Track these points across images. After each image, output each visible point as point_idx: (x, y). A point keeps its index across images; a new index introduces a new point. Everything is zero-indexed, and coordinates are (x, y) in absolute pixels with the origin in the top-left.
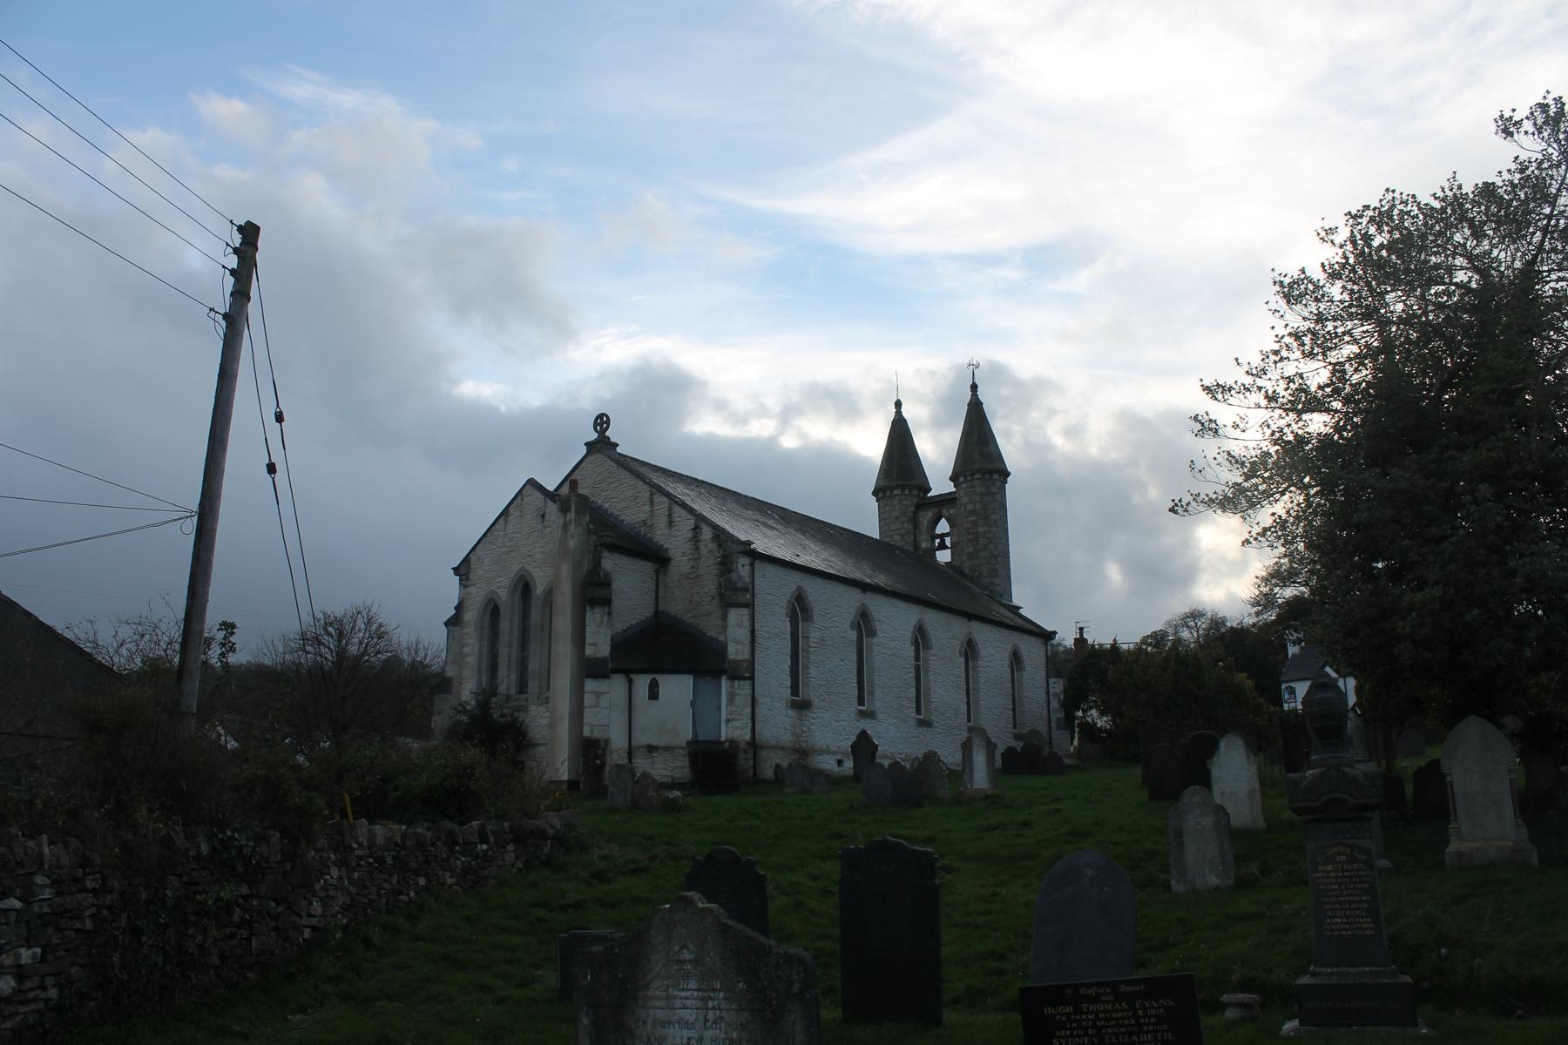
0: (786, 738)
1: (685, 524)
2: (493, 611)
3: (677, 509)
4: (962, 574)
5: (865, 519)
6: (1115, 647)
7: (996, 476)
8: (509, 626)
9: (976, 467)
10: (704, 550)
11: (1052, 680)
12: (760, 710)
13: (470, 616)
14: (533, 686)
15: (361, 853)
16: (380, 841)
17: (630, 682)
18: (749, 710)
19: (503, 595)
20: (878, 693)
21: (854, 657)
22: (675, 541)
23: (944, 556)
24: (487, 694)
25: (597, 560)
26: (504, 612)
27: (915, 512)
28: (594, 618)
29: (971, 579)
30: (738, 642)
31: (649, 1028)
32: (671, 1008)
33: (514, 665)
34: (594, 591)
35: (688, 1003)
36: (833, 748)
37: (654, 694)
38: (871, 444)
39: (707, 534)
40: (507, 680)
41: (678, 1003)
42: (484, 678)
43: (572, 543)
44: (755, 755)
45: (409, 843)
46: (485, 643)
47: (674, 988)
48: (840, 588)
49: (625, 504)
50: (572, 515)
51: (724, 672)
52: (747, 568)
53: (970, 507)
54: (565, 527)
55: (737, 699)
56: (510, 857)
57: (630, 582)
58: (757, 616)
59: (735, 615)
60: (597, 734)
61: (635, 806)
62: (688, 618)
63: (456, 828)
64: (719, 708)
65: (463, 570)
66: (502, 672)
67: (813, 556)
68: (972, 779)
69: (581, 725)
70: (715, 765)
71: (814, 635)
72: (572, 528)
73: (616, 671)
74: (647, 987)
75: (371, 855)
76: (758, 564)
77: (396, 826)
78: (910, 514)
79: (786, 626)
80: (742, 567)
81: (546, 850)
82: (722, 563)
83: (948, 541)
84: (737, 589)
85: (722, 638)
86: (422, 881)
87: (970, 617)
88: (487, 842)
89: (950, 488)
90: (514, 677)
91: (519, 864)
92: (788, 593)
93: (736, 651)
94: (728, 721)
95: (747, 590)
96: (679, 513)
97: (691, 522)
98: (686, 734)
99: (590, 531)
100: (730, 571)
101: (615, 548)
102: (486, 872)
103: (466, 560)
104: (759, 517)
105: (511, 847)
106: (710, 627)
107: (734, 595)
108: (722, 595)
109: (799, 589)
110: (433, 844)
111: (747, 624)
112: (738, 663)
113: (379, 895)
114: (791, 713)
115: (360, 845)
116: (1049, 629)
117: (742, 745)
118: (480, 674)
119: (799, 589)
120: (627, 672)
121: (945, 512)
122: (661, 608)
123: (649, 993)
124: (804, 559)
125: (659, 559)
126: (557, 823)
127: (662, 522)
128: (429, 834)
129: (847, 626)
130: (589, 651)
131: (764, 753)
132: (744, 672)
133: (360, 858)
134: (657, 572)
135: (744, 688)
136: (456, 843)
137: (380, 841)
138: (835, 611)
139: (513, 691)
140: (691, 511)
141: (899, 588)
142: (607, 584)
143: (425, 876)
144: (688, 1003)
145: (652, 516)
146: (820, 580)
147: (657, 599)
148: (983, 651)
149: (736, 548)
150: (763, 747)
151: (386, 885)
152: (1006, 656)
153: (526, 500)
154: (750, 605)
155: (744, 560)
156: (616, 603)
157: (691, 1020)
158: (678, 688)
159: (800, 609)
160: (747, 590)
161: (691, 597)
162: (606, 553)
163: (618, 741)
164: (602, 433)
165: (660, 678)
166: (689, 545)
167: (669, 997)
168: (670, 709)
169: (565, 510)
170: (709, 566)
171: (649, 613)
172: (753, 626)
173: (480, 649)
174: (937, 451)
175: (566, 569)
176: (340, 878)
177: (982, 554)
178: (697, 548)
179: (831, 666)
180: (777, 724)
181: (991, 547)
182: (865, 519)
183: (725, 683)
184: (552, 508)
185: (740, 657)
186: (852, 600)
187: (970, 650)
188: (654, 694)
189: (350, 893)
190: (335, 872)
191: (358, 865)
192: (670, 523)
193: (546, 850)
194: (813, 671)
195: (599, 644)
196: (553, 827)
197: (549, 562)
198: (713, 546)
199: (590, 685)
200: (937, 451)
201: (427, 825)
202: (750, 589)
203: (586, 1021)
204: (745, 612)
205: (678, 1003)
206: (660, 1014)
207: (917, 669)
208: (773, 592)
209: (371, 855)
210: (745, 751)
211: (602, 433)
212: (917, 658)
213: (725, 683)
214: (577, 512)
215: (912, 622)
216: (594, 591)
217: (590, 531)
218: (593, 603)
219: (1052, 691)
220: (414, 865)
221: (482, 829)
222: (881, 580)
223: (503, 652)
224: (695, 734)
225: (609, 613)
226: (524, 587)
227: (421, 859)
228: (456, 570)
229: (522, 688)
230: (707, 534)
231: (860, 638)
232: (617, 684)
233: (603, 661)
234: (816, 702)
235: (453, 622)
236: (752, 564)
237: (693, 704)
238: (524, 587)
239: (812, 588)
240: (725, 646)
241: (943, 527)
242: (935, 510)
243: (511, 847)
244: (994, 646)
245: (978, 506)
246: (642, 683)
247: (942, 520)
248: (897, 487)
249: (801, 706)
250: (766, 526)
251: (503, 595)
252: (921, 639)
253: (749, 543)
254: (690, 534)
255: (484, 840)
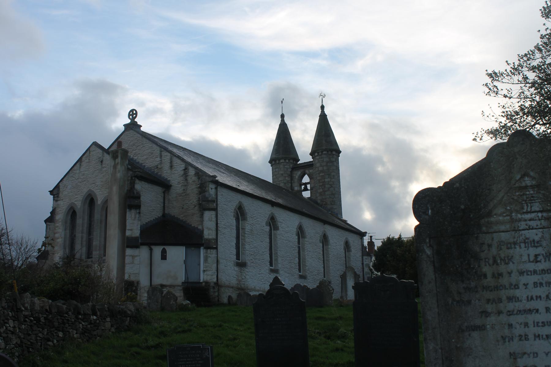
0: (234, 282)
1: (179, 167)
2: (72, 213)
3: (175, 159)
4: (316, 203)
5: (266, 174)
6: (400, 238)
7: (334, 153)
8: (81, 222)
9: (324, 148)
10: (190, 181)
11: (365, 257)
12: (221, 266)
13: (59, 217)
14: (96, 254)
15: (27, 313)
16: (37, 307)
17: (151, 250)
18: (215, 265)
19: (79, 205)
20: (280, 260)
21: (268, 240)
22: (174, 177)
23: (306, 194)
24: (69, 259)
25: (132, 184)
26: (79, 214)
27: (291, 172)
28: (131, 215)
29: (321, 206)
30: (209, 229)
31: (494, 251)
32: (516, 230)
33: (84, 243)
34: (131, 201)
35: (533, 224)
36: (258, 288)
37: (164, 257)
38: (264, 139)
39: (192, 172)
40: (80, 250)
41: (523, 225)
42: (67, 250)
43: (119, 175)
44: (218, 290)
45: (53, 311)
46: (68, 231)
47: (517, 212)
48: (260, 203)
49: (147, 159)
50: (119, 160)
51: (202, 245)
52: (214, 190)
53: (321, 169)
54: (115, 167)
55: (209, 259)
56: (108, 325)
57: (149, 195)
58: (219, 216)
59: (208, 215)
60: (133, 278)
61: (162, 309)
62: (181, 217)
63: (79, 305)
64: (199, 265)
65: (55, 192)
66: (78, 247)
67: (244, 186)
68: (347, 295)
69: (123, 274)
70: (198, 294)
71: (248, 228)
72: (119, 167)
73: (143, 244)
74: (489, 214)
75: (32, 315)
76: (219, 189)
77: (46, 300)
78: (289, 173)
79: (234, 222)
80: (211, 190)
81: (127, 323)
82: (200, 187)
83: (309, 187)
84: (208, 201)
85: (200, 227)
86: (61, 334)
87: (325, 222)
88: (96, 316)
89: (310, 159)
90: (84, 249)
91: (113, 330)
92: (234, 205)
93: (208, 234)
94: (204, 271)
95: (214, 201)
96: (176, 161)
97: (183, 166)
98: (181, 278)
99: (128, 169)
100: (205, 191)
101: (142, 178)
102: (95, 333)
103: (57, 187)
104: (215, 167)
105: (108, 319)
106: (194, 221)
107: (207, 204)
108: (200, 204)
109: (240, 203)
110: (67, 313)
111: (214, 219)
112: (209, 240)
113: (36, 340)
114: (236, 268)
115: (26, 309)
116: (363, 231)
117: (212, 284)
118: (65, 248)
119: (240, 203)
120: (150, 245)
121: (307, 171)
122: (166, 212)
123: (492, 219)
124: (242, 188)
125: (165, 186)
126: (132, 308)
127: (166, 166)
128: (65, 307)
129: (264, 224)
130: (128, 233)
131: (222, 290)
132: (211, 245)
133: (26, 317)
134: (164, 192)
135: (212, 254)
136: (79, 313)
137: (37, 307)
138: (258, 214)
139: (84, 257)
140: (183, 160)
141: (292, 206)
142: (139, 197)
143: (62, 331)
144: (533, 224)
145: (161, 163)
146: (250, 199)
147: (164, 207)
148: (331, 241)
149: (208, 179)
150: (221, 286)
151: (40, 335)
152: (342, 243)
153: (92, 153)
154: (215, 209)
155: (212, 186)
156: (143, 208)
157: (537, 238)
158: (177, 254)
159: (240, 213)
160: (214, 201)
161: (183, 207)
162: (137, 181)
163: (144, 282)
164: (133, 120)
165: (166, 247)
166: (182, 178)
167: (513, 221)
168: (172, 266)
169: (115, 157)
170: (193, 189)
171: (160, 214)
172: (217, 221)
173: (65, 235)
174: (304, 139)
175: (115, 189)
176: (14, 327)
177: (327, 193)
178: (186, 180)
179: (256, 245)
180: (229, 274)
181: (332, 189)
182: (266, 174)
183: (202, 251)
184: (108, 158)
185: (210, 237)
186: (267, 210)
187: (325, 240)
188: (164, 257)
189: (19, 337)
190: (11, 323)
191: (25, 321)
192: (171, 167)
193: (127, 323)
194: (247, 247)
195: (134, 230)
196: (130, 311)
197: (105, 186)
198: (194, 178)
199: (129, 251)
200: (304, 139)
201: (62, 301)
202: (215, 201)
203: (429, 252)
204: (213, 213)
205: (523, 225)
206: (504, 236)
207: (299, 248)
208: (227, 204)
209: (32, 315)
210: (214, 288)
211: (133, 120)
212: (299, 243)
213: (202, 251)
214: (122, 158)
215: (297, 224)
216: (131, 201)
217: (128, 169)
218: (131, 207)
219: (365, 263)
220: (56, 324)
221: (94, 306)
222: (280, 201)
223: (78, 235)
224: (187, 277)
225: (139, 213)
226: (91, 200)
227: (60, 321)
228: (51, 192)
229: (89, 255)
230: (192, 172)
231: (271, 230)
232: (144, 252)
233: (136, 239)
234: (249, 263)
235: (49, 221)
236: (216, 188)
237: (185, 262)
238: (91, 200)
239: (247, 203)
240: (202, 232)
241: (306, 179)
242: (302, 170)
243: (108, 319)
244: (337, 239)
245: (325, 168)
246: (157, 251)
247: (308, 176)
248: (282, 158)
249: (241, 265)
250: (220, 172)
251: (79, 205)
252: (301, 232)
253: (215, 177)
254: (182, 172)
255: (95, 314)
